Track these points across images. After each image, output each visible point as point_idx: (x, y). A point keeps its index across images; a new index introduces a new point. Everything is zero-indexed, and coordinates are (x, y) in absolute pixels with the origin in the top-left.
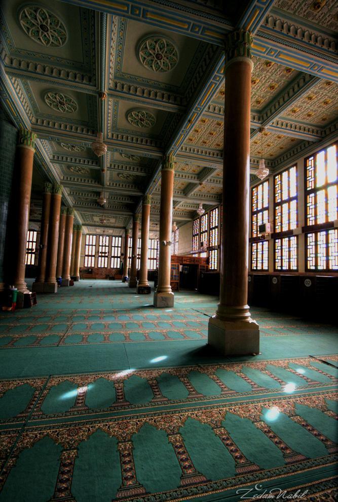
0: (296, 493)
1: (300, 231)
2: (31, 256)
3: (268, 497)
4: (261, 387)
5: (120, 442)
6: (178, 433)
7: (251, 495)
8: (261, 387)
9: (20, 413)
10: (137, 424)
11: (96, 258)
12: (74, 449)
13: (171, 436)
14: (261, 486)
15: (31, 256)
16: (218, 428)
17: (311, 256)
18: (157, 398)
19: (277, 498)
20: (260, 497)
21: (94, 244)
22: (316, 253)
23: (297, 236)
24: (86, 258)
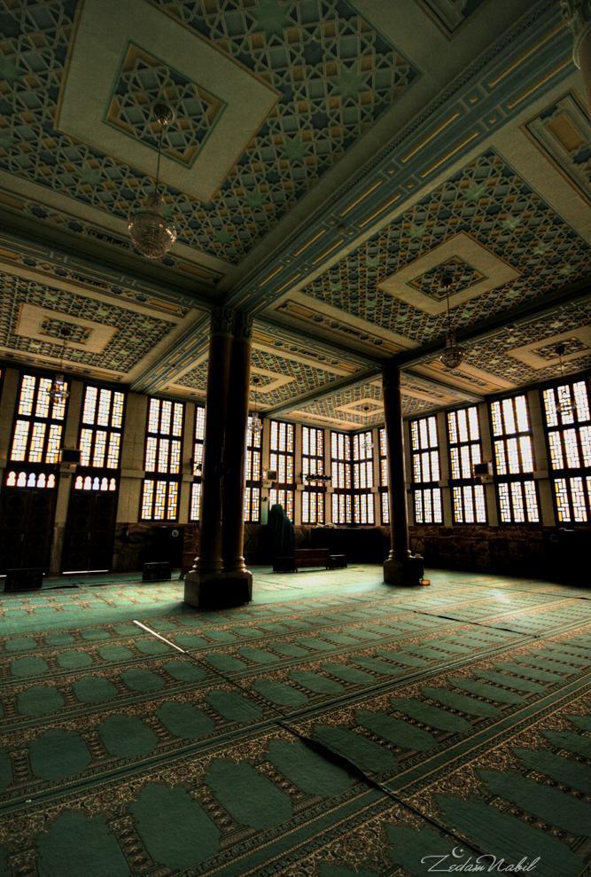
0: (520, 863)
1: (375, 490)
3: (474, 869)
4: (320, 694)
5: (110, 820)
6: (203, 785)
7: (446, 864)
9: (8, 787)
10: (132, 788)
11: (185, 488)
13: (111, 823)
16: (196, 788)
19: (489, 870)
20: (461, 869)
22: (345, 516)
23: (374, 494)
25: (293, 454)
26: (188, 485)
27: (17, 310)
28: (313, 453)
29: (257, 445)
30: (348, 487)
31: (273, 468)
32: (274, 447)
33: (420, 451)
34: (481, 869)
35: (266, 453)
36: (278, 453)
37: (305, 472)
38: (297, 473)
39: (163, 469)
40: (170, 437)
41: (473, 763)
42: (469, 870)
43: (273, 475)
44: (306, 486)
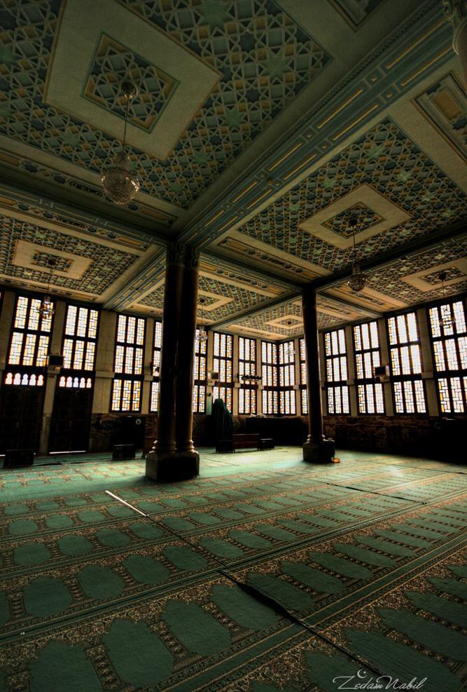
1: (297, 387)
2: (72, 364)
3: (375, 687)
4: (253, 549)
5: (87, 649)
6: (161, 620)
7: (352, 683)
8: (253, 549)
10: (104, 623)
11: (146, 385)
12: (23, 671)
13: (88, 651)
14: (365, 672)
15: (72, 364)
16: (155, 623)
17: (443, 388)
18: (15, 619)
20: (364, 687)
21: (375, 345)
23: (295, 390)
24: (118, 383)
25: (232, 359)
26: (149, 383)
27: (13, 245)
28: (247, 358)
29: (203, 352)
30: (275, 385)
31: (216, 370)
32: (216, 354)
33: (332, 357)
34: (380, 687)
35: (210, 358)
36: (219, 358)
37: (241, 373)
38: (235, 374)
39: (128, 371)
40: (135, 346)
41: (374, 604)
42: (371, 688)
43: (216, 376)
44: (242, 385)
